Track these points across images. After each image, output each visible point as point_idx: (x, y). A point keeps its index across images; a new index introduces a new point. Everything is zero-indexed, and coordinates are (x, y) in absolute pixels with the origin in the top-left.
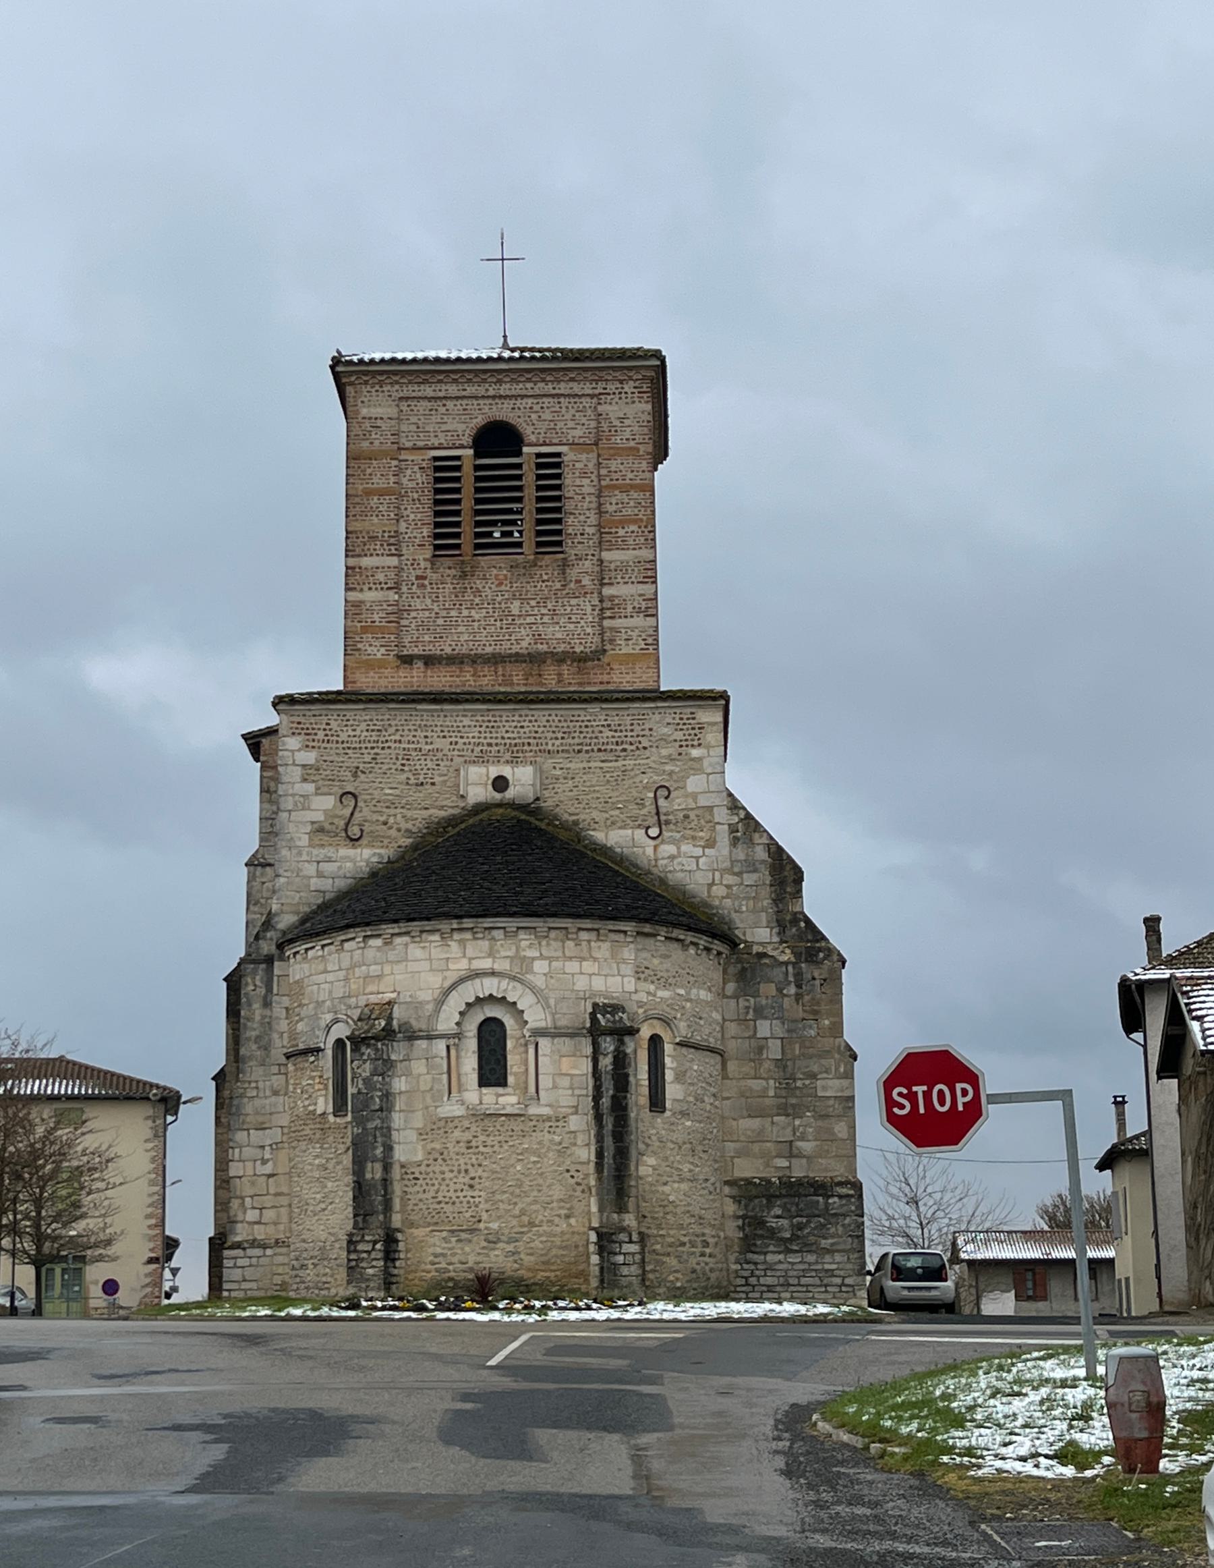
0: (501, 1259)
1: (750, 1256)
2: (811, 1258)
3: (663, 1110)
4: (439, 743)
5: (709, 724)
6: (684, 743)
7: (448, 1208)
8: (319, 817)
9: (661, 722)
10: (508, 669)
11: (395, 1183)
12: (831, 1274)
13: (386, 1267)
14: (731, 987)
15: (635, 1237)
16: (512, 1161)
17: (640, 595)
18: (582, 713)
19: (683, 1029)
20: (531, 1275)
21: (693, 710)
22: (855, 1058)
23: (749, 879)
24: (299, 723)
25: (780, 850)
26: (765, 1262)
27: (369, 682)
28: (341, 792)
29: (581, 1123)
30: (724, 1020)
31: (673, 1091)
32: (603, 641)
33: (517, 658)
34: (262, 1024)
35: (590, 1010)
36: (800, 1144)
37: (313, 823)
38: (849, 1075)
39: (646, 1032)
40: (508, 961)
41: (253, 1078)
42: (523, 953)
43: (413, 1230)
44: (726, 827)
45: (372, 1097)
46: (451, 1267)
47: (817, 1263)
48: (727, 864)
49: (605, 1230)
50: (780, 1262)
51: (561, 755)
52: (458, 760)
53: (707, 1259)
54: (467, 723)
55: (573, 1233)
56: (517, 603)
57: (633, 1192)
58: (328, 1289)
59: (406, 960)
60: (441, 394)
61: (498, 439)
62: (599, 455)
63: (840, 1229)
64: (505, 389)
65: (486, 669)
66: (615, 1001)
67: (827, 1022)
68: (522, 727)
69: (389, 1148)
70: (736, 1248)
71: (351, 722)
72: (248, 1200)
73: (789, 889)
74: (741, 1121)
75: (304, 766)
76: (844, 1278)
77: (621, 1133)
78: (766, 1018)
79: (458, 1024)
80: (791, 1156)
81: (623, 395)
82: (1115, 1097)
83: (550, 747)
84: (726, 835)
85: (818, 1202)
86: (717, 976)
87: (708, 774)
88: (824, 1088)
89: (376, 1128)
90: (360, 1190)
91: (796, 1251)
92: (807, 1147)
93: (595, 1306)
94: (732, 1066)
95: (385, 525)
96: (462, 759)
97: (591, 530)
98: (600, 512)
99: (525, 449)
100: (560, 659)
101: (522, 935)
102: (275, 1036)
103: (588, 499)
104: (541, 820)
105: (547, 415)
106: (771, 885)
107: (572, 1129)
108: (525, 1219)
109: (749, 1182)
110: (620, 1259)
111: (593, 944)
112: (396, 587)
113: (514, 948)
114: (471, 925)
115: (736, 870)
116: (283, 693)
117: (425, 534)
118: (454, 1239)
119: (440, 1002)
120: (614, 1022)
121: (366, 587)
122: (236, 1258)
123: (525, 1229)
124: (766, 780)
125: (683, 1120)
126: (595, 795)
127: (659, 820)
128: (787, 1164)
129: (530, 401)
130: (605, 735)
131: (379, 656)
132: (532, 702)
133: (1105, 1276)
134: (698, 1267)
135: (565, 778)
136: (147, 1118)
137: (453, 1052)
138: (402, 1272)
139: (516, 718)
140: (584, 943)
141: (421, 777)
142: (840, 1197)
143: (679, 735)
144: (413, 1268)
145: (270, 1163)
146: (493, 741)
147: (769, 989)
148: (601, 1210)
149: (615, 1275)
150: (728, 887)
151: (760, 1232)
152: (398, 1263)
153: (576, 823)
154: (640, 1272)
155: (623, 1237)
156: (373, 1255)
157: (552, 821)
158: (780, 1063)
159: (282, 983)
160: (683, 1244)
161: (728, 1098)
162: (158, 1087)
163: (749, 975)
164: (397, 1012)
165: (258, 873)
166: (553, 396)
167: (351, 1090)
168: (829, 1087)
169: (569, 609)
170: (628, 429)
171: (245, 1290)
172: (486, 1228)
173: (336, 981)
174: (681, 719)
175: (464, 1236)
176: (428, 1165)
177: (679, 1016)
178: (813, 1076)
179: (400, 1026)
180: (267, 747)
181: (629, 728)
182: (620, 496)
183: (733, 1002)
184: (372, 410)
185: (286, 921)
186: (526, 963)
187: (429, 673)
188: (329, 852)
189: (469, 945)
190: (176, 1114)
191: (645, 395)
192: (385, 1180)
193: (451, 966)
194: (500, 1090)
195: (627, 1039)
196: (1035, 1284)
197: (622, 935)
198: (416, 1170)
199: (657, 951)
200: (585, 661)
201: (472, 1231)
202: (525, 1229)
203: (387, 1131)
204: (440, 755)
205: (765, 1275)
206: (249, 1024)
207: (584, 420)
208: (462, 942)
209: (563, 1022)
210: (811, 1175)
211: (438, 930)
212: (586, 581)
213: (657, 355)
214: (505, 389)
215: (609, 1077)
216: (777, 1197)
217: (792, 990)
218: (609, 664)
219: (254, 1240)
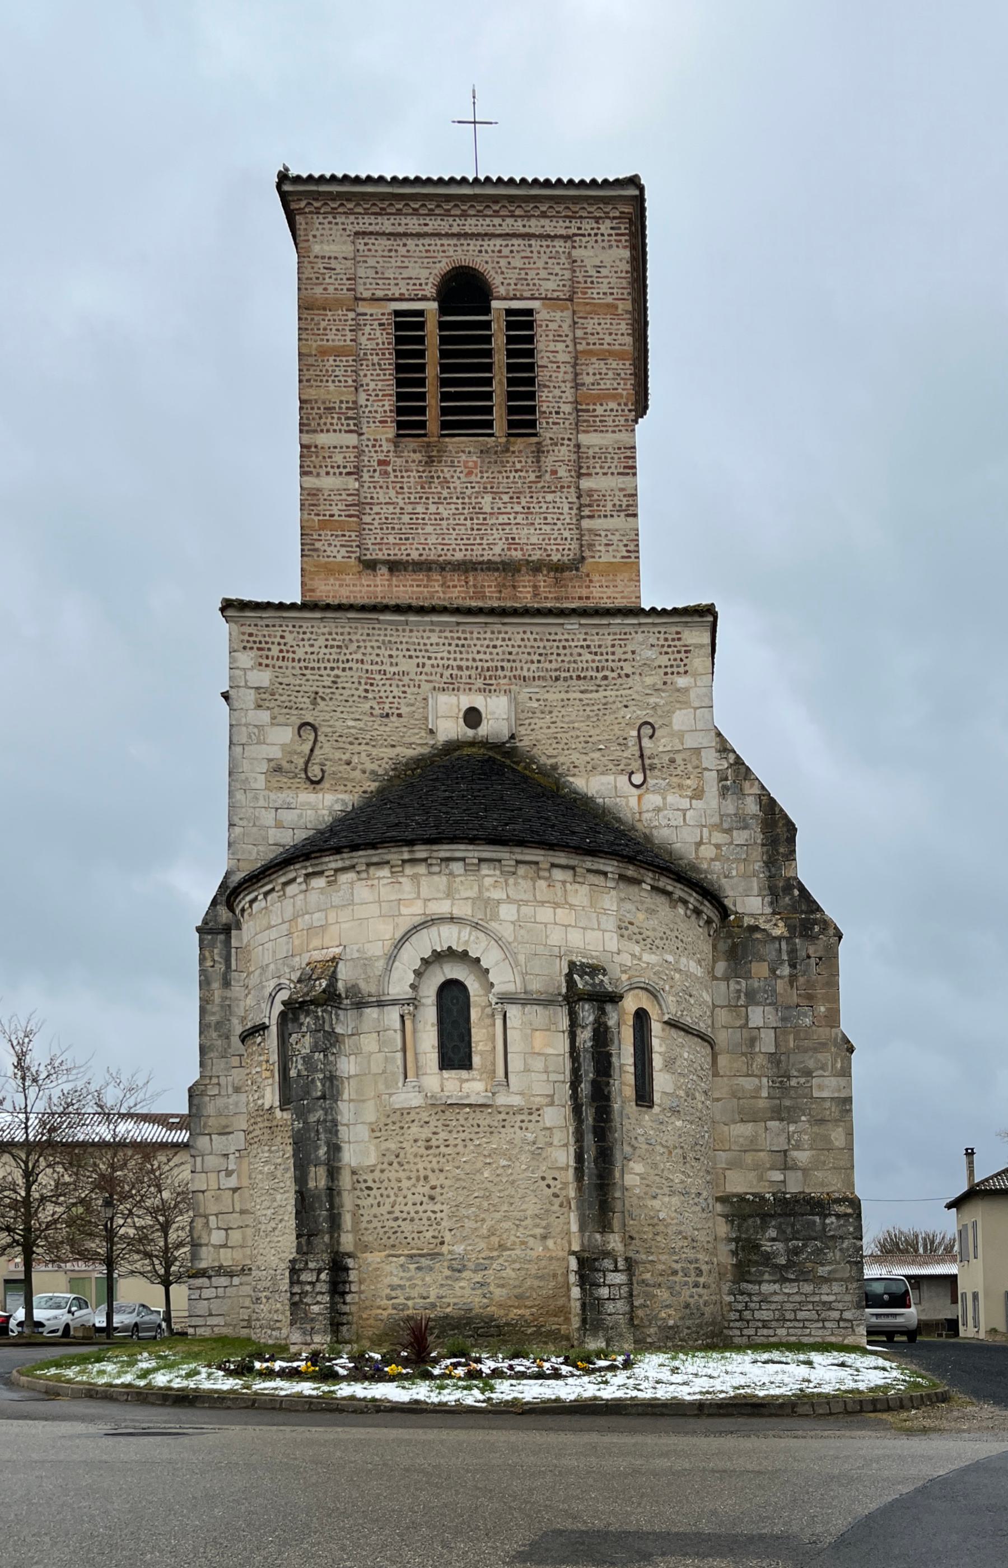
0: (468, 1292)
1: (744, 1285)
2: (807, 1288)
4: (407, 665)
6: (669, 670)
7: (406, 1226)
8: (276, 753)
9: (644, 644)
10: (480, 578)
12: (828, 1306)
13: (333, 1303)
14: (721, 967)
15: (621, 1264)
16: (479, 1165)
17: (621, 490)
18: (559, 630)
19: (672, 1007)
20: (502, 1312)
21: (679, 629)
22: (851, 1050)
23: (740, 837)
24: (251, 635)
25: (772, 802)
26: (760, 1294)
27: (328, 590)
28: (299, 722)
29: (557, 1117)
30: (714, 1006)
31: (662, 1082)
32: (581, 546)
33: (490, 566)
34: (222, 1006)
35: (566, 971)
36: (795, 1154)
37: (270, 760)
38: (846, 1072)
39: (630, 1004)
41: (214, 1073)
42: (487, 894)
43: (368, 1255)
44: (715, 773)
45: (313, 1079)
46: (410, 1303)
47: (814, 1294)
48: (716, 819)
49: (586, 1255)
50: (775, 1293)
51: (537, 683)
52: (426, 687)
53: (700, 1290)
54: (433, 638)
55: (551, 1258)
56: (488, 498)
57: (618, 1206)
58: (280, 1329)
59: (352, 903)
60: (401, 230)
61: (464, 290)
62: (574, 312)
63: (838, 1254)
64: (471, 225)
65: (456, 578)
66: (595, 961)
67: (823, 1009)
68: (495, 647)
69: (335, 1149)
70: (729, 1276)
71: (308, 635)
72: (212, 1218)
73: (782, 850)
74: (732, 1126)
75: (257, 688)
76: (842, 1311)
77: (603, 1128)
78: (758, 1004)
80: (785, 1168)
81: (599, 238)
82: (967, 1150)
83: (525, 673)
84: (715, 783)
85: (815, 1222)
86: (707, 948)
87: (696, 709)
88: (820, 1087)
89: (318, 1121)
90: (304, 1203)
92: (802, 1157)
93: (565, 1369)
94: (723, 1061)
95: (342, 393)
96: (431, 685)
97: (567, 408)
98: (577, 386)
99: (495, 304)
100: (536, 568)
103: (563, 369)
106: (763, 845)
107: (548, 1125)
108: (495, 1240)
109: (742, 1198)
110: (604, 1292)
111: (568, 885)
112: (356, 472)
113: (476, 888)
115: (726, 826)
117: (387, 408)
118: (412, 1267)
119: (392, 958)
120: (593, 985)
121: (323, 472)
122: (200, 1288)
123: (495, 1254)
124: (758, 699)
126: (574, 733)
127: (643, 765)
128: (781, 1178)
129: (499, 242)
131: (339, 559)
133: (925, 1288)
134: (691, 1300)
137: (408, 1023)
138: (354, 1309)
139: (488, 635)
140: (558, 885)
142: (838, 1216)
143: (664, 660)
144: (368, 1303)
145: (235, 1175)
146: (464, 664)
147: (760, 969)
148: (582, 1229)
149: (599, 1313)
150: (718, 846)
151: (755, 1258)
152: (349, 1298)
153: (554, 767)
154: (627, 1309)
155: (608, 1264)
157: (529, 764)
158: (774, 1059)
159: (240, 956)
160: (675, 1273)
161: (718, 1100)
163: (740, 952)
164: (344, 973)
168: (825, 1087)
169: (545, 506)
171: (212, 1326)
172: (450, 1252)
174: (666, 640)
175: (425, 1262)
176: (382, 1171)
177: (667, 988)
178: (808, 1073)
179: (347, 991)
181: (610, 650)
183: (723, 985)
184: (326, 247)
186: (490, 906)
187: (394, 581)
189: (424, 881)
191: (623, 238)
192: (330, 1189)
193: (404, 911)
194: (464, 1074)
195: (609, 1008)
197: (602, 878)
198: (369, 1177)
200: (563, 571)
201: (434, 1256)
202: (495, 1254)
203: (333, 1127)
204: (406, 679)
205: (760, 1309)
207: (557, 269)
208: (415, 877)
209: (535, 985)
210: (807, 1191)
211: (388, 862)
212: (562, 472)
213: (636, 176)
214: (471, 225)
215: (589, 1056)
216: (772, 1216)
217: (785, 970)
218: (588, 575)
219: (220, 1267)
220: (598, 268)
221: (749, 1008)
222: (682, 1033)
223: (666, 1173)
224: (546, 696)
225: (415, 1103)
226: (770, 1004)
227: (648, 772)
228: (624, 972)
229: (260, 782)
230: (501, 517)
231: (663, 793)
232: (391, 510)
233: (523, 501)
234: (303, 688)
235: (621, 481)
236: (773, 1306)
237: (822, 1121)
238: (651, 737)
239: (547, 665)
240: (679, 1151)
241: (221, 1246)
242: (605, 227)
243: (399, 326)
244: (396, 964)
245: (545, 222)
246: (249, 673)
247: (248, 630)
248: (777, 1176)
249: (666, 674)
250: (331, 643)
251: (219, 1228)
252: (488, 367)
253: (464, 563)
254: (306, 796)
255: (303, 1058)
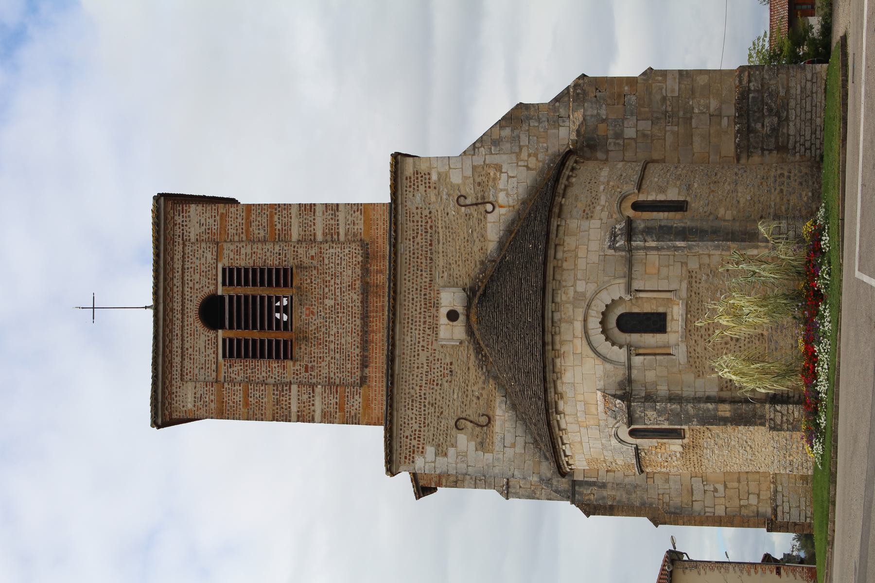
1: (790, 146)
2: (792, 103)
3: (685, 202)
5: (414, 167)
9: (414, 200)
11: (733, 395)
12: (803, 90)
13: (794, 403)
18: (404, 256)
19: (629, 188)
23: (524, 141)
24: (406, 458)
25: (504, 118)
26: (795, 136)
27: (379, 407)
28: (455, 429)
30: (623, 160)
31: (672, 195)
32: (354, 241)
33: (365, 302)
35: (612, 252)
36: (712, 109)
37: (477, 450)
40: (576, 310)
41: (656, 497)
45: (671, 410)
47: (796, 99)
50: (795, 125)
51: (433, 273)
53: (792, 175)
54: (409, 338)
56: (327, 301)
59: (573, 384)
60: (180, 351)
61: (212, 312)
62: (225, 241)
63: (772, 82)
67: (626, 88)
68: (413, 299)
72: (742, 503)
74: (695, 151)
78: (623, 131)
79: (621, 347)
80: (720, 116)
81: (184, 223)
85: (753, 97)
87: (450, 168)
88: (673, 91)
91: (788, 112)
92: (714, 104)
94: (656, 156)
95: (269, 393)
97: (277, 248)
98: (265, 241)
99: (220, 293)
100: (366, 271)
101: (558, 300)
102: (627, 480)
103: (255, 250)
104: (479, 287)
105: (197, 277)
109: (737, 146)
112: (313, 386)
113: (568, 305)
114: (550, 336)
115: (517, 150)
116: (384, 468)
117: (276, 365)
119: (605, 359)
121: (312, 408)
125: (693, 189)
126: (463, 249)
128: (726, 118)
129: (186, 289)
130: (420, 241)
131: (360, 400)
132: (395, 292)
135: (450, 270)
136: (684, 573)
137: (641, 351)
139: (406, 303)
140: (565, 255)
141: (446, 372)
143: (422, 188)
146: (422, 320)
148: (757, 247)
150: (529, 155)
152: (791, 395)
153: (482, 263)
156: (785, 412)
157: (478, 278)
159: (589, 475)
162: (664, 566)
165: (513, 491)
166: (183, 273)
167: (666, 426)
168: (672, 87)
170: (208, 220)
173: (592, 436)
174: (410, 186)
178: (664, 99)
180: (425, 482)
181: (415, 224)
182: (254, 227)
183: (611, 154)
185: (546, 469)
188: (497, 439)
190: (682, 554)
192: (731, 402)
193: (579, 351)
194: (669, 318)
196: (804, 4)
197: (560, 228)
199: (572, 204)
200: (368, 254)
204: (431, 358)
205: (804, 136)
206: (618, 498)
207: (201, 252)
210: (734, 102)
212: (313, 252)
213: (158, 198)
214: (177, 306)
220: (201, 225)
221: (625, 137)
222: (644, 181)
223: (725, 194)
224: (441, 267)
225: (685, 349)
226: (623, 123)
227: (486, 200)
228: (612, 217)
229: (489, 456)
230: (337, 294)
231: (497, 190)
232: (333, 365)
233: (329, 278)
234: (436, 425)
235: (319, 213)
236: (803, 126)
237: (693, 91)
238: (465, 198)
239: (424, 264)
240: (712, 185)
241: (759, 498)
242: (179, 219)
243: (231, 356)
244: (608, 357)
245: (176, 257)
246: (427, 460)
247: (403, 460)
248: (725, 121)
249: (430, 187)
250: (410, 406)
251: (748, 499)
252: (254, 298)
253: (362, 319)
254: (497, 426)
255: (659, 416)
